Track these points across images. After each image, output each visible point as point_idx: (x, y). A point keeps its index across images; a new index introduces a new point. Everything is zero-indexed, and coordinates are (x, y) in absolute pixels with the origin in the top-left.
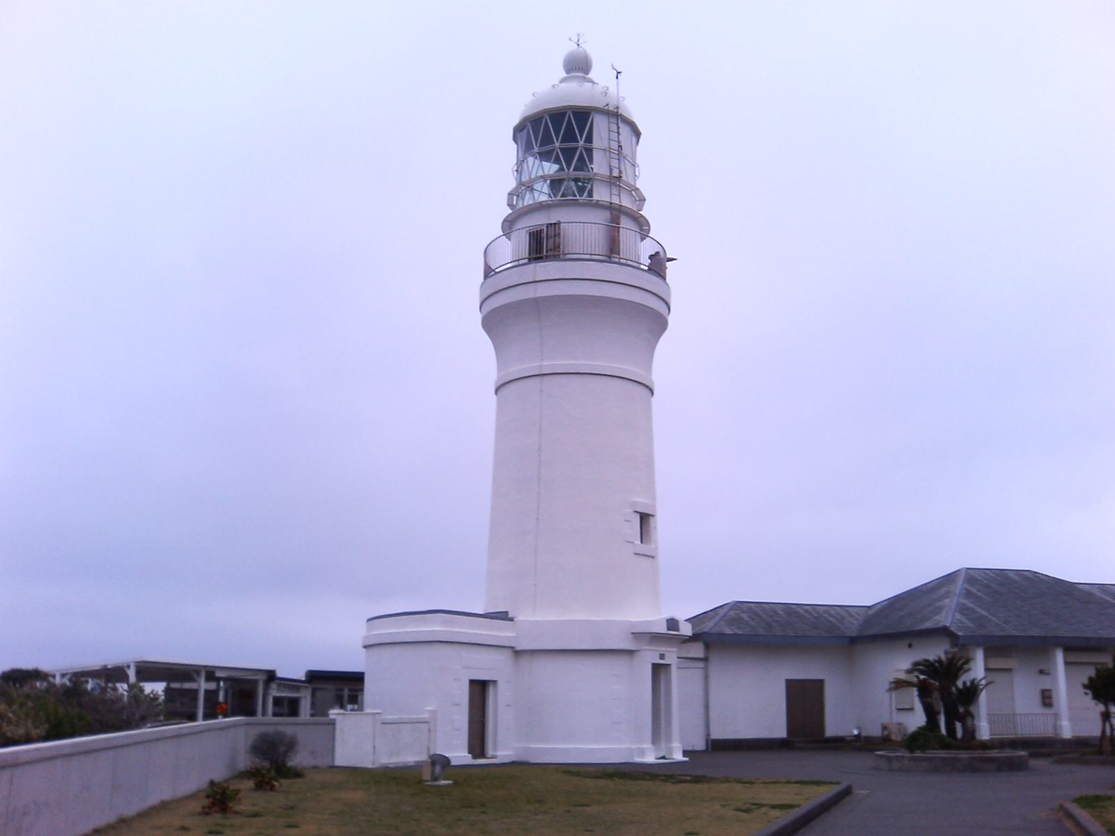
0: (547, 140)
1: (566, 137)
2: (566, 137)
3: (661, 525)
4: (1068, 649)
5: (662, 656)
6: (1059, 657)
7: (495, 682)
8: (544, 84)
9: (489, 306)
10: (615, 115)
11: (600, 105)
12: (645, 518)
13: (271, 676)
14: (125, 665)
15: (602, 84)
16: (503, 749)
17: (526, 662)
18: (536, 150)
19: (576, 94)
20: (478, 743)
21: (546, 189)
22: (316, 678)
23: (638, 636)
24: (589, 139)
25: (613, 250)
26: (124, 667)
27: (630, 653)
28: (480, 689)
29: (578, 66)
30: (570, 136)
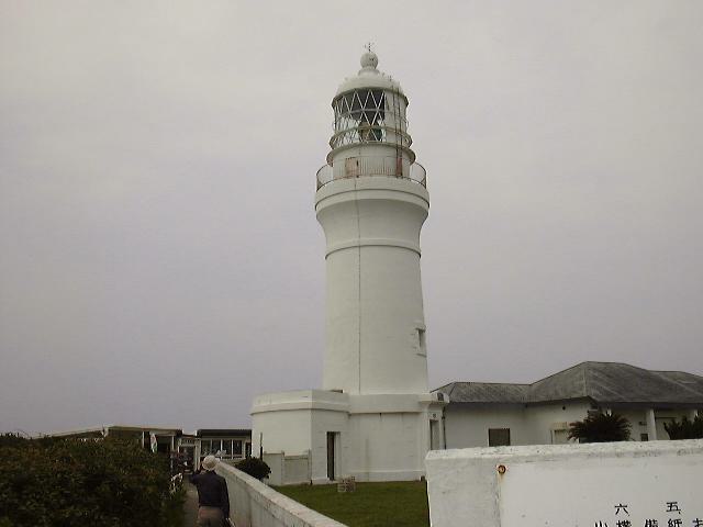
0: (356, 106)
1: (369, 107)
2: (369, 107)
3: (428, 335)
4: (656, 410)
5: (434, 415)
6: (652, 414)
7: (339, 433)
8: (350, 75)
9: (320, 207)
10: (398, 94)
11: (388, 86)
12: (421, 332)
13: (179, 434)
14: (283, 436)
15: (392, 71)
16: (344, 472)
17: (354, 420)
18: (350, 112)
19: (370, 80)
20: (331, 474)
21: (357, 135)
22: (202, 433)
23: (421, 404)
24: (382, 106)
25: (399, 173)
26: (367, 55)
27: (417, 413)
28: (331, 436)
29: (371, 62)
30: (370, 104)
